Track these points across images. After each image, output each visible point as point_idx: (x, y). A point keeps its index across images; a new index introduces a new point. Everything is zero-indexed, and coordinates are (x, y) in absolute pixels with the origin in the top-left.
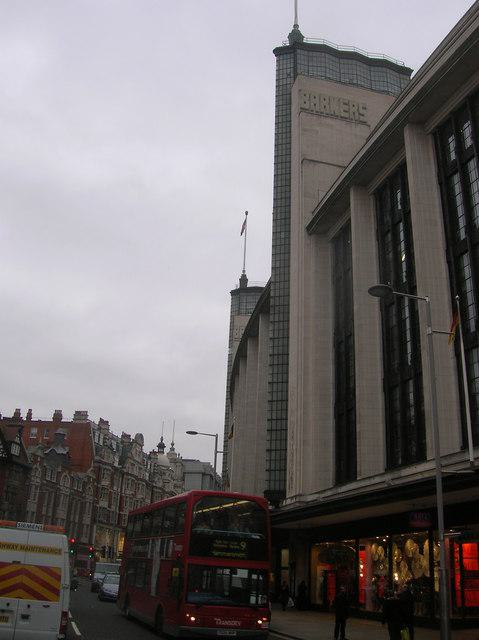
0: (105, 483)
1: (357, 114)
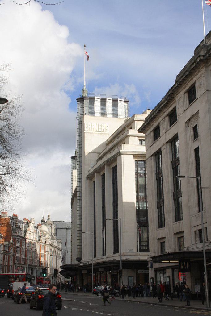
0: (18, 245)
1: (104, 129)
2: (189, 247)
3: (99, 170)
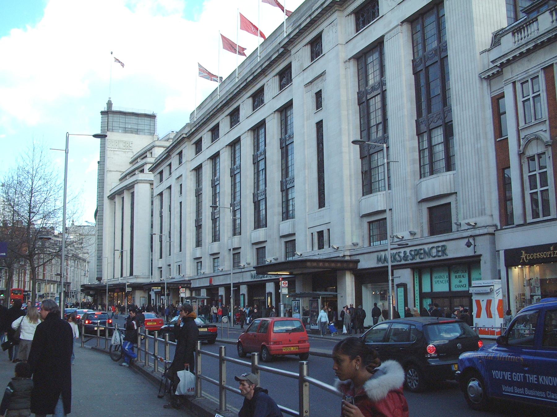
2: (303, 255)
3: (120, 192)
